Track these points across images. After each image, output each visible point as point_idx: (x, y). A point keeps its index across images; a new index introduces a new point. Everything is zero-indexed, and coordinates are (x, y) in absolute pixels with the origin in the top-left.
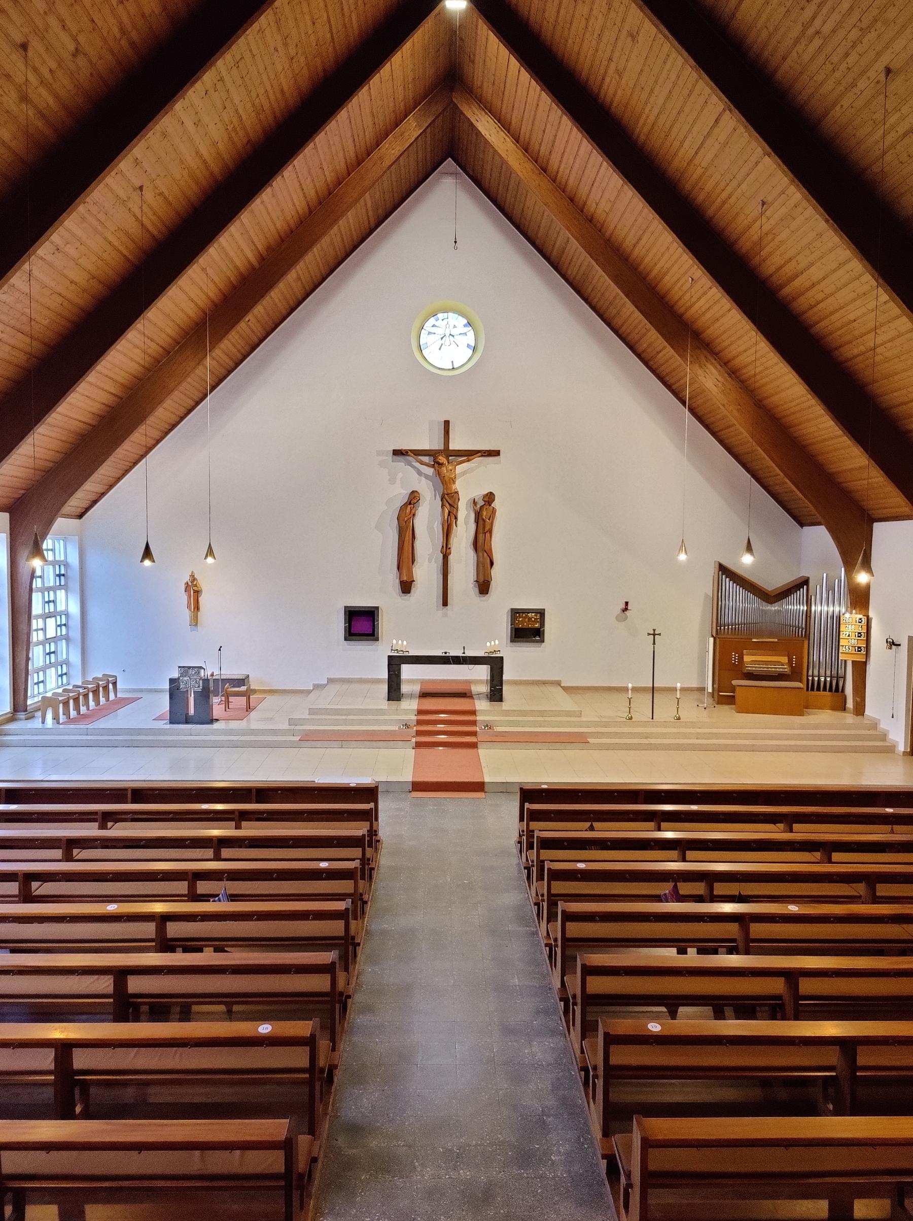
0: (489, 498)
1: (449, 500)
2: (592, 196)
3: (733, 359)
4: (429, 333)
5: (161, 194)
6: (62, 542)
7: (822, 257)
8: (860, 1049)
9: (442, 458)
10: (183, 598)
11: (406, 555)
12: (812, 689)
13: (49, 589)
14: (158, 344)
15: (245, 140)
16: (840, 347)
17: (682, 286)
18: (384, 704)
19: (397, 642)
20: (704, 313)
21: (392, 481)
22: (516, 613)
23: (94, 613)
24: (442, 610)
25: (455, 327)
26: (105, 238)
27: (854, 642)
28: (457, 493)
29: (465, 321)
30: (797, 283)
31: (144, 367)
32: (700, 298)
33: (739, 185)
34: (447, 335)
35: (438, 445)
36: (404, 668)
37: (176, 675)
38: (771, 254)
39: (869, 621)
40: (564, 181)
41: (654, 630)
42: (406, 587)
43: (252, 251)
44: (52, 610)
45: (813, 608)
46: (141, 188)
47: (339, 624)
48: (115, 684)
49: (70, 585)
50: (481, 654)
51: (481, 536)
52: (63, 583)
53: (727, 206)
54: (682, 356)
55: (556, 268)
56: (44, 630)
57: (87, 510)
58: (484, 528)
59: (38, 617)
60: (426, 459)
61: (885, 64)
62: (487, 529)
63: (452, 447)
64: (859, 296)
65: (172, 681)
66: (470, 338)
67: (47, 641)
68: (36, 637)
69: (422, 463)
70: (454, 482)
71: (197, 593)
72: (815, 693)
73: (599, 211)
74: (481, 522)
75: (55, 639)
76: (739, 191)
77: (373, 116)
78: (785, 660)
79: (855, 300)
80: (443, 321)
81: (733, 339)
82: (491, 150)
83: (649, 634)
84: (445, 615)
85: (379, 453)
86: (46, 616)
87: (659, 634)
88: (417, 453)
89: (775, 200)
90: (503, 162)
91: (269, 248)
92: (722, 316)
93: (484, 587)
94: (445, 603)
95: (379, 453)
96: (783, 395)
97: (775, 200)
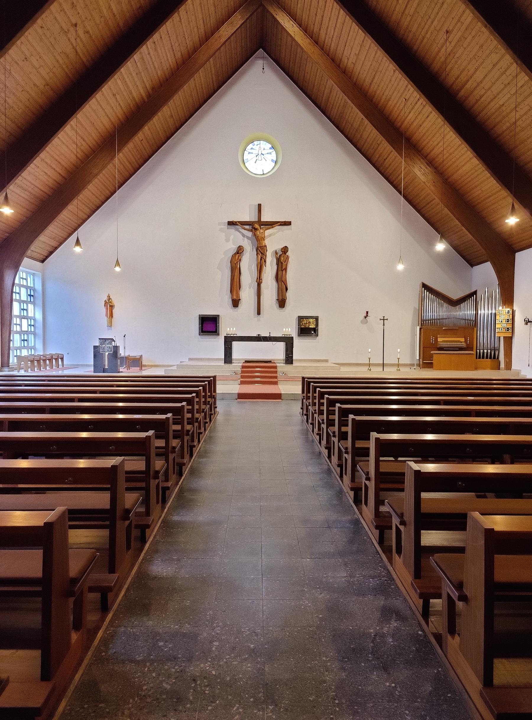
0: (285, 250)
1: (261, 250)
2: (345, 53)
3: (430, 153)
4: (249, 153)
5: (88, 32)
6: (32, 276)
7: (483, 63)
9: (257, 227)
10: (103, 310)
12: (480, 358)
13: (24, 302)
14: (87, 144)
15: (138, 6)
17: (399, 107)
18: (222, 363)
19: (230, 329)
21: (227, 240)
22: (301, 319)
23: (50, 319)
24: (256, 319)
25: (264, 149)
26: (54, 56)
27: (505, 325)
28: (266, 246)
30: (468, 86)
32: (410, 112)
33: (432, 23)
34: (260, 154)
36: (235, 344)
38: (452, 68)
39: (513, 312)
40: (328, 49)
41: (384, 317)
42: (236, 303)
43: (143, 87)
44: (25, 314)
45: (479, 312)
46: (76, 25)
47: (195, 325)
48: (62, 359)
49: (37, 302)
50: (279, 335)
51: (280, 273)
52: (32, 300)
53: (425, 40)
55: (324, 113)
56: (20, 325)
57: (47, 257)
59: (17, 316)
60: (247, 227)
62: (284, 268)
63: (263, 219)
64: (506, 86)
65: (95, 347)
66: (274, 156)
67: (21, 332)
68: (15, 328)
70: (264, 240)
71: (112, 307)
72: (481, 360)
73: (349, 64)
74: (280, 264)
75: (27, 332)
76: (433, 26)
77: (215, 7)
78: (463, 340)
79: (503, 90)
80: (257, 150)
81: (429, 138)
82: (285, 34)
83: (381, 319)
84: (259, 320)
85: (220, 224)
86: (22, 318)
87: (387, 319)
89: (454, 27)
90: (293, 39)
91: (153, 89)
92: (423, 123)
93: (282, 303)
94: (259, 313)
95: (220, 224)
96: (460, 171)
97: (454, 27)
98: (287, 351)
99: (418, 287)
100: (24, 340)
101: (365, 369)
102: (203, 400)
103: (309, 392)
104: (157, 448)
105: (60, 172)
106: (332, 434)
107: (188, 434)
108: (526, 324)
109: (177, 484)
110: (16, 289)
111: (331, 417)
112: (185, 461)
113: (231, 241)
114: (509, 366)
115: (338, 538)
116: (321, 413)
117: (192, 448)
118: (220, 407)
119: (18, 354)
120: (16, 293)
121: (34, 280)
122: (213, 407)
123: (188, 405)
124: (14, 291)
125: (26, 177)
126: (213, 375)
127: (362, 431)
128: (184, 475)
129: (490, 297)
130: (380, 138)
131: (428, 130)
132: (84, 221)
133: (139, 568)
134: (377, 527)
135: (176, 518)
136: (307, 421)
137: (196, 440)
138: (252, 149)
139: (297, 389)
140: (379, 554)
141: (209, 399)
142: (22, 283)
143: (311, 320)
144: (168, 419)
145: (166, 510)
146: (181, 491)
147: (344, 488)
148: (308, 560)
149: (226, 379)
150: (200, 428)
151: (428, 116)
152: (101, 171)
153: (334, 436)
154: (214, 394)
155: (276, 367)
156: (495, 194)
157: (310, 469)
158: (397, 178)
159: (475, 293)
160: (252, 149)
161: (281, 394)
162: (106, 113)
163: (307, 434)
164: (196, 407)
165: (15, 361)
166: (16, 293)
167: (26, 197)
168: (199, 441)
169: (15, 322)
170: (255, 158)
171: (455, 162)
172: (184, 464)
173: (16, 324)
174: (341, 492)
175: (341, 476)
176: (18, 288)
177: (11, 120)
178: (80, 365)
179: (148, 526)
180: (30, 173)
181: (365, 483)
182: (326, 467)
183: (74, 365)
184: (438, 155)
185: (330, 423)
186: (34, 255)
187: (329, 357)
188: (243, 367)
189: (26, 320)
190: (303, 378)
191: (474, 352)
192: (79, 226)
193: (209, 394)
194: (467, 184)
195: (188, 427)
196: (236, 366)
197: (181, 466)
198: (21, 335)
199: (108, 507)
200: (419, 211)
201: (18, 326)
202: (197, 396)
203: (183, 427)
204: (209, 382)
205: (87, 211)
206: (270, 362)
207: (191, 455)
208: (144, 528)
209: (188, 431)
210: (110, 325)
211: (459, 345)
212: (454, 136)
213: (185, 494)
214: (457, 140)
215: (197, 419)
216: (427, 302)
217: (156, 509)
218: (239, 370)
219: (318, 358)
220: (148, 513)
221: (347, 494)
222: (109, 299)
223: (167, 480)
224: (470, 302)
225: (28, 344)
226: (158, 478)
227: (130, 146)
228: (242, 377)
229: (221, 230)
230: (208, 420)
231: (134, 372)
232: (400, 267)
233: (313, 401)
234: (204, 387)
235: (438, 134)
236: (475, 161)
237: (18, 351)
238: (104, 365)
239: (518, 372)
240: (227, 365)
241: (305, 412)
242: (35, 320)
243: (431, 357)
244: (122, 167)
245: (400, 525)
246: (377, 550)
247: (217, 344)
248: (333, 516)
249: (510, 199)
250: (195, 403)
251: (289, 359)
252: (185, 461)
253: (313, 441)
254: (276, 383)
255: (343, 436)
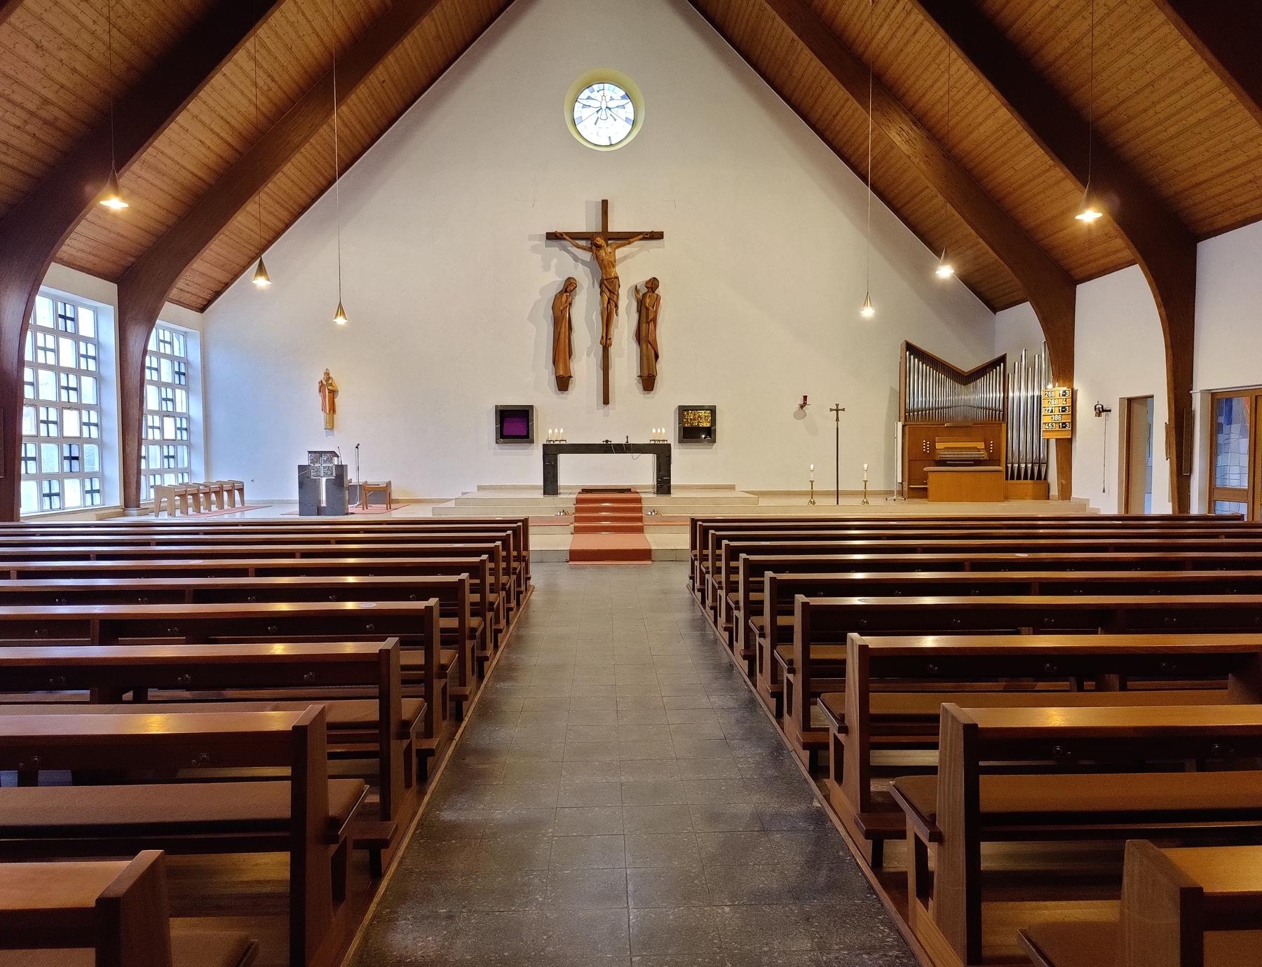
0: (653, 285)
1: (608, 286)
4: (584, 106)
8: (1219, 483)
9: (600, 242)
10: (317, 400)
11: (562, 350)
12: (1012, 478)
13: (167, 385)
16: (1042, 47)
18: (539, 494)
20: (886, 45)
21: (546, 268)
22: (683, 410)
23: (218, 416)
24: (602, 410)
28: (617, 278)
29: (623, 93)
31: (265, 116)
32: (881, 26)
35: (593, 226)
36: (563, 459)
37: (305, 461)
39: (1074, 393)
42: (563, 383)
44: (170, 409)
45: (1011, 394)
47: (489, 425)
48: (241, 490)
49: (192, 385)
50: (645, 440)
51: (644, 326)
54: (864, 104)
56: (161, 429)
57: (210, 302)
58: (647, 316)
59: (153, 413)
60: (583, 243)
61: (862, 837)
63: (614, 227)
65: (302, 468)
67: (163, 442)
69: (578, 247)
71: (333, 393)
72: (1015, 481)
74: (644, 311)
75: (173, 442)
78: (981, 445)
80: (603, 121)
84: (606, 415)
85: (531, 238)
86: (164, 415)
88: (575, 236)
93: (648, 382)
94: (606, 401)
95: (531, 238)
96: (975, 135)
98: (659, 470)
99: (898, 351)
100: (168, 457)
101: (805, 501)
102: (504, 565)
103: (705, 546)
104: (404, 668)
105: (230, 140)
106: (757, 632)
107: (472, 637)
108: (1099, 414)
109: (452, 739)
110: (150, 361)
111: (754, 596)
112: (468, 690)
113: (553, 269)
114: (1066, 492)
115: (784, 856)
116: (732, 587)
117: (481, 662)
118: (537, 576)
119: (158, 483)
120: (150, 368)
121: (186, 346)
122: (523, 578)
123: (471, 577)
124: (148, 364)
125: (161, 147)
126: (521, 516)
127: (828, 626)
128: (467, 719)
129: (1031, 365)
130: (826, 74)
131: (915, 59)
132: (278, 234)
133: (365, 939)
134: (867, 835)
135: (448, 815)
136: (703, 602)
137: (490, 646)
138: (589, 98)
139: (682, 540)
140: (875, 893)
141: (514, 564)
142: (162, 351)
143: (702, 413)
144: (429, 609)
145: (426, 799)
146: (461, 752)
147: (785, 740)
148: (727, 909)
149: (547, 523)
150: (497, 621)
151: (915, 32)
152: (306, 139)
153: (762, 635)
154: (524, 553)
155: (639, 500)
156: (1039, 175)
157: (716, 700)
158: (858, 149)
159: (1003, 359)
160: (589, 98)
161: (650, 551)
162: (314, 29)
163: (704, 629)
164: (490, 579)
165: (152, 496)
166: (150, 368)
167: (165, 188)
168: (496, 647)
169: (150, 423)
170: (596, 115)
171: (967, 115)
172: (466, 698)
173: (153, 427)
174: (778, 750)
175: (779, 715)
176: (154, 359)
177: (131, 40)
178: (274, 501)
179: (385, 843)
180: (171, 142)
181: (835, 736)
182: (744, 695)
183: (265, 502)
184: (935, 104)
185: (754, 609)
186: (186, 297)
187: (745, 478)
188: (579, 501)
189: (172, 420)
190: (694, 522)
191: (1002, 468)
192: (270, 243)
193: (515, 553)
194: (986, 158)
195: (474, 622)
196: (566, 499)
197: (460, 700)
198: (162, 448)
199: (286, 813)
200: (896, 211)
201: (157, 431)
202: (491, 559)
203: (462, 622)
204: (515, 530)
205: (285, 215)
206: (628, 490)
207: (481, 676)
208: (376, 849)
209: (473, 630)
210: (331, 426)
211: (975, 455)
212: (966, 67)
213: (467, 760)
214: (971, 74)
215: (492, 604)
216: (914, 377)
217: (403, 798)
218: (571, 506)
219: (718, 481)
220: (384, 811)
221: (793, 754)
222: (328, 378)
223: (428, 733)
224: (994, 377)
225: (176, 463)
226: (408, 737)
227: (362, 91)
228: (577, 519)
229: (534, 249)
230: (513, 604)
231: (376, 513)
232: (868, 312)
233: (714, 564)
234: (505, 541)
235: (934, 66)
236: (1004, 114)
237: (158, 477)
238: (320, 501)
239: (1084, 504)
240: (550, 498)
241: (697, 585)
242: (188, 419)
243: (924, 477)
244: (347, 132)
245: (930, 841)
246: (868, 882)
247: (529, 461)
248: (772, 805)
249: (1070, 184)
250: (487, 572)
251: (664, 485)
252: (468, 690)
253: (716, 641)
254: (640, 530)
255: (782, 636)
